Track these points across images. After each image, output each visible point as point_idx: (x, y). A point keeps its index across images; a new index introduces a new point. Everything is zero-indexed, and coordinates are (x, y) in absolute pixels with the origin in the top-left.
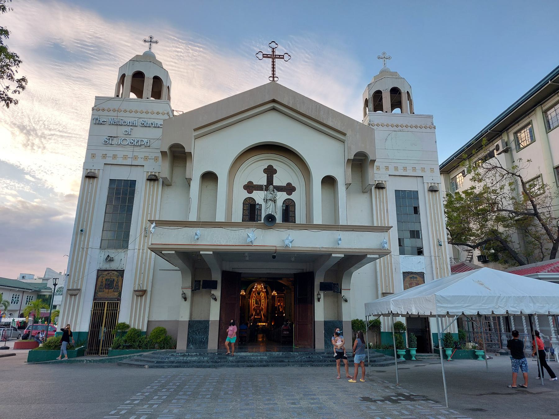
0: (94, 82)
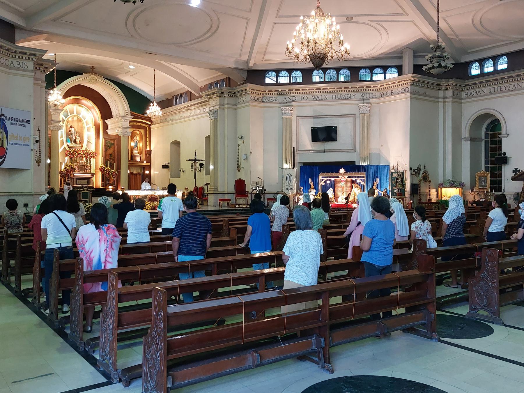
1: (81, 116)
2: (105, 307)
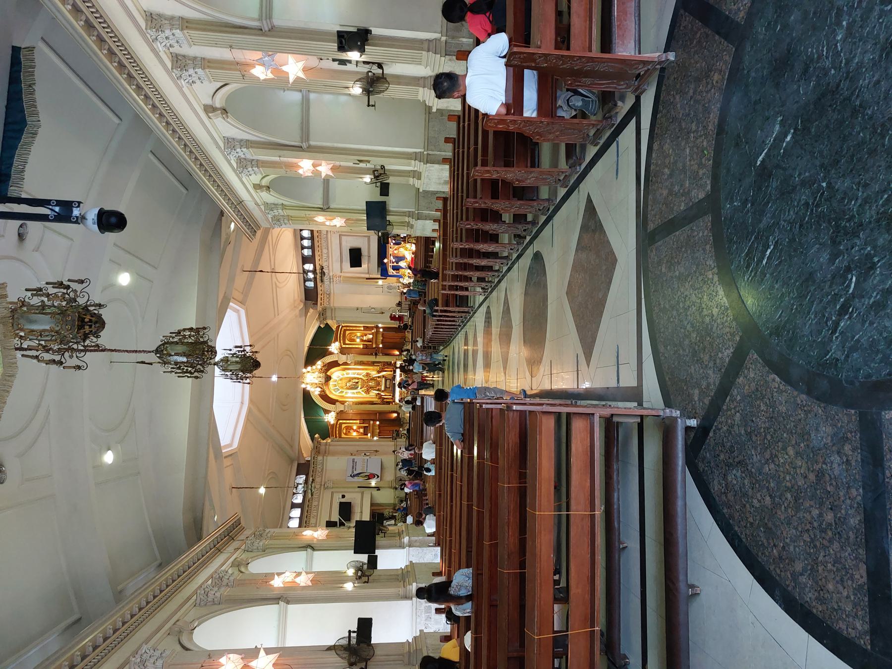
0: (510, 445)
1: (338, 379)
2: (735, 476)
